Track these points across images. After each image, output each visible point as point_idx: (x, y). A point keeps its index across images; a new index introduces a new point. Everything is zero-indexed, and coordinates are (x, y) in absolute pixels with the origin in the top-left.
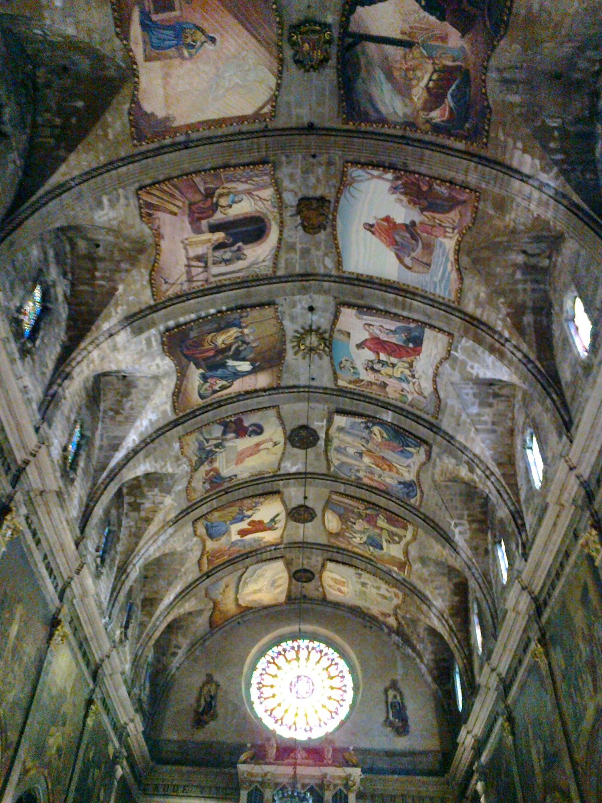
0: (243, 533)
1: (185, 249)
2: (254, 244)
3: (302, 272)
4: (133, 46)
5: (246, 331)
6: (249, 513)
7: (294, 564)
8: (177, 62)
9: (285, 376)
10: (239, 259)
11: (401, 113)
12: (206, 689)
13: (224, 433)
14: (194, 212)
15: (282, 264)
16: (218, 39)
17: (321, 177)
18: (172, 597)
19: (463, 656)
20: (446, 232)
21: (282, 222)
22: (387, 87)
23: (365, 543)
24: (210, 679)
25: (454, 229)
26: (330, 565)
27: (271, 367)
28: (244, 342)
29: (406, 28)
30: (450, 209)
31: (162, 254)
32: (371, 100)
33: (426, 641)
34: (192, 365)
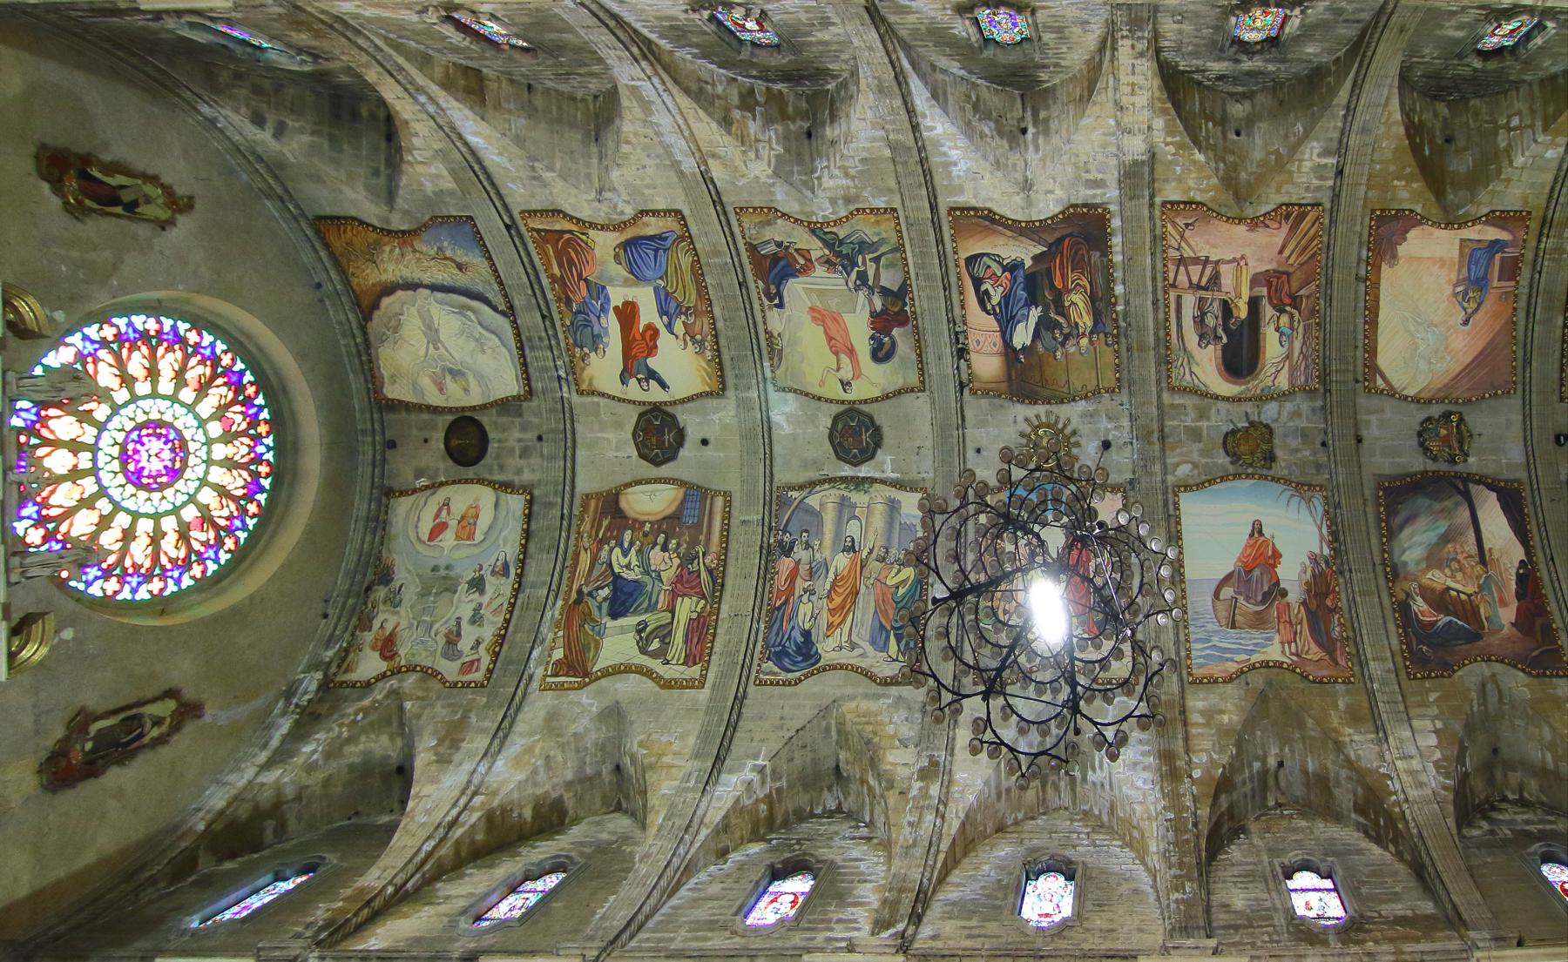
0: (628, 314)
1: (1234, 260)
2: (1220, 361)
3: (1167, 430)
4: (1478, 227)
5: (1084, 342)
6: (679, 327)
7: (503, 420)
8: (1454, 276)
9: (984, 402)
10: (1202, 337)
11: (1404, 558)
12: (149, 189)
13: (885, 292)
14: (1278, 278)
15: (1178, 400)
16: (1467, 328)
17: (1299, 455)
18: (473, 140)
19: (398, 880)
20: (1289, 643)
21: (1240, 400)
22: (1432, 536)
23: (617, 577)
24: (180, 204)
25: (1297, 654)
26: (516, 503)
27: (1010, 379)
28: (1067, 337)
29: (1496, 555)
30: (1320, 644)
31: (1228, 226)
32: (1410, 519)
33: (334, 765)
34: (1040, 249)
